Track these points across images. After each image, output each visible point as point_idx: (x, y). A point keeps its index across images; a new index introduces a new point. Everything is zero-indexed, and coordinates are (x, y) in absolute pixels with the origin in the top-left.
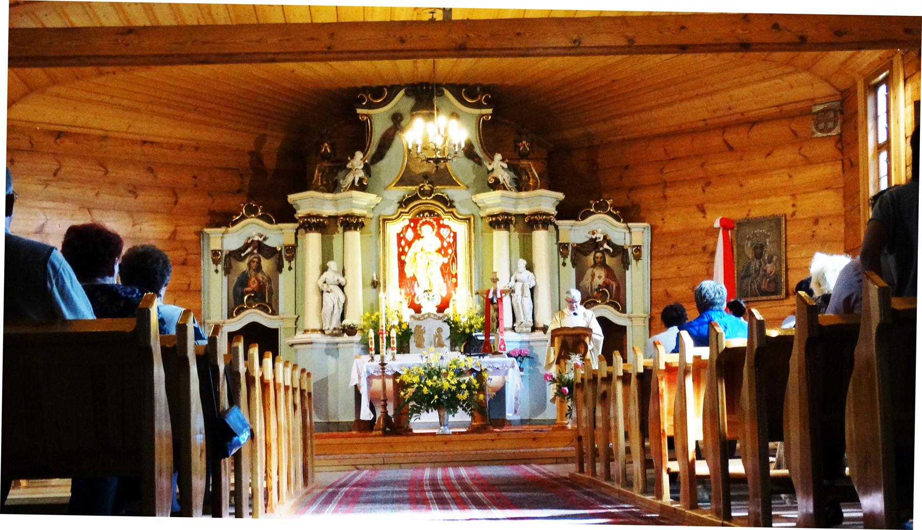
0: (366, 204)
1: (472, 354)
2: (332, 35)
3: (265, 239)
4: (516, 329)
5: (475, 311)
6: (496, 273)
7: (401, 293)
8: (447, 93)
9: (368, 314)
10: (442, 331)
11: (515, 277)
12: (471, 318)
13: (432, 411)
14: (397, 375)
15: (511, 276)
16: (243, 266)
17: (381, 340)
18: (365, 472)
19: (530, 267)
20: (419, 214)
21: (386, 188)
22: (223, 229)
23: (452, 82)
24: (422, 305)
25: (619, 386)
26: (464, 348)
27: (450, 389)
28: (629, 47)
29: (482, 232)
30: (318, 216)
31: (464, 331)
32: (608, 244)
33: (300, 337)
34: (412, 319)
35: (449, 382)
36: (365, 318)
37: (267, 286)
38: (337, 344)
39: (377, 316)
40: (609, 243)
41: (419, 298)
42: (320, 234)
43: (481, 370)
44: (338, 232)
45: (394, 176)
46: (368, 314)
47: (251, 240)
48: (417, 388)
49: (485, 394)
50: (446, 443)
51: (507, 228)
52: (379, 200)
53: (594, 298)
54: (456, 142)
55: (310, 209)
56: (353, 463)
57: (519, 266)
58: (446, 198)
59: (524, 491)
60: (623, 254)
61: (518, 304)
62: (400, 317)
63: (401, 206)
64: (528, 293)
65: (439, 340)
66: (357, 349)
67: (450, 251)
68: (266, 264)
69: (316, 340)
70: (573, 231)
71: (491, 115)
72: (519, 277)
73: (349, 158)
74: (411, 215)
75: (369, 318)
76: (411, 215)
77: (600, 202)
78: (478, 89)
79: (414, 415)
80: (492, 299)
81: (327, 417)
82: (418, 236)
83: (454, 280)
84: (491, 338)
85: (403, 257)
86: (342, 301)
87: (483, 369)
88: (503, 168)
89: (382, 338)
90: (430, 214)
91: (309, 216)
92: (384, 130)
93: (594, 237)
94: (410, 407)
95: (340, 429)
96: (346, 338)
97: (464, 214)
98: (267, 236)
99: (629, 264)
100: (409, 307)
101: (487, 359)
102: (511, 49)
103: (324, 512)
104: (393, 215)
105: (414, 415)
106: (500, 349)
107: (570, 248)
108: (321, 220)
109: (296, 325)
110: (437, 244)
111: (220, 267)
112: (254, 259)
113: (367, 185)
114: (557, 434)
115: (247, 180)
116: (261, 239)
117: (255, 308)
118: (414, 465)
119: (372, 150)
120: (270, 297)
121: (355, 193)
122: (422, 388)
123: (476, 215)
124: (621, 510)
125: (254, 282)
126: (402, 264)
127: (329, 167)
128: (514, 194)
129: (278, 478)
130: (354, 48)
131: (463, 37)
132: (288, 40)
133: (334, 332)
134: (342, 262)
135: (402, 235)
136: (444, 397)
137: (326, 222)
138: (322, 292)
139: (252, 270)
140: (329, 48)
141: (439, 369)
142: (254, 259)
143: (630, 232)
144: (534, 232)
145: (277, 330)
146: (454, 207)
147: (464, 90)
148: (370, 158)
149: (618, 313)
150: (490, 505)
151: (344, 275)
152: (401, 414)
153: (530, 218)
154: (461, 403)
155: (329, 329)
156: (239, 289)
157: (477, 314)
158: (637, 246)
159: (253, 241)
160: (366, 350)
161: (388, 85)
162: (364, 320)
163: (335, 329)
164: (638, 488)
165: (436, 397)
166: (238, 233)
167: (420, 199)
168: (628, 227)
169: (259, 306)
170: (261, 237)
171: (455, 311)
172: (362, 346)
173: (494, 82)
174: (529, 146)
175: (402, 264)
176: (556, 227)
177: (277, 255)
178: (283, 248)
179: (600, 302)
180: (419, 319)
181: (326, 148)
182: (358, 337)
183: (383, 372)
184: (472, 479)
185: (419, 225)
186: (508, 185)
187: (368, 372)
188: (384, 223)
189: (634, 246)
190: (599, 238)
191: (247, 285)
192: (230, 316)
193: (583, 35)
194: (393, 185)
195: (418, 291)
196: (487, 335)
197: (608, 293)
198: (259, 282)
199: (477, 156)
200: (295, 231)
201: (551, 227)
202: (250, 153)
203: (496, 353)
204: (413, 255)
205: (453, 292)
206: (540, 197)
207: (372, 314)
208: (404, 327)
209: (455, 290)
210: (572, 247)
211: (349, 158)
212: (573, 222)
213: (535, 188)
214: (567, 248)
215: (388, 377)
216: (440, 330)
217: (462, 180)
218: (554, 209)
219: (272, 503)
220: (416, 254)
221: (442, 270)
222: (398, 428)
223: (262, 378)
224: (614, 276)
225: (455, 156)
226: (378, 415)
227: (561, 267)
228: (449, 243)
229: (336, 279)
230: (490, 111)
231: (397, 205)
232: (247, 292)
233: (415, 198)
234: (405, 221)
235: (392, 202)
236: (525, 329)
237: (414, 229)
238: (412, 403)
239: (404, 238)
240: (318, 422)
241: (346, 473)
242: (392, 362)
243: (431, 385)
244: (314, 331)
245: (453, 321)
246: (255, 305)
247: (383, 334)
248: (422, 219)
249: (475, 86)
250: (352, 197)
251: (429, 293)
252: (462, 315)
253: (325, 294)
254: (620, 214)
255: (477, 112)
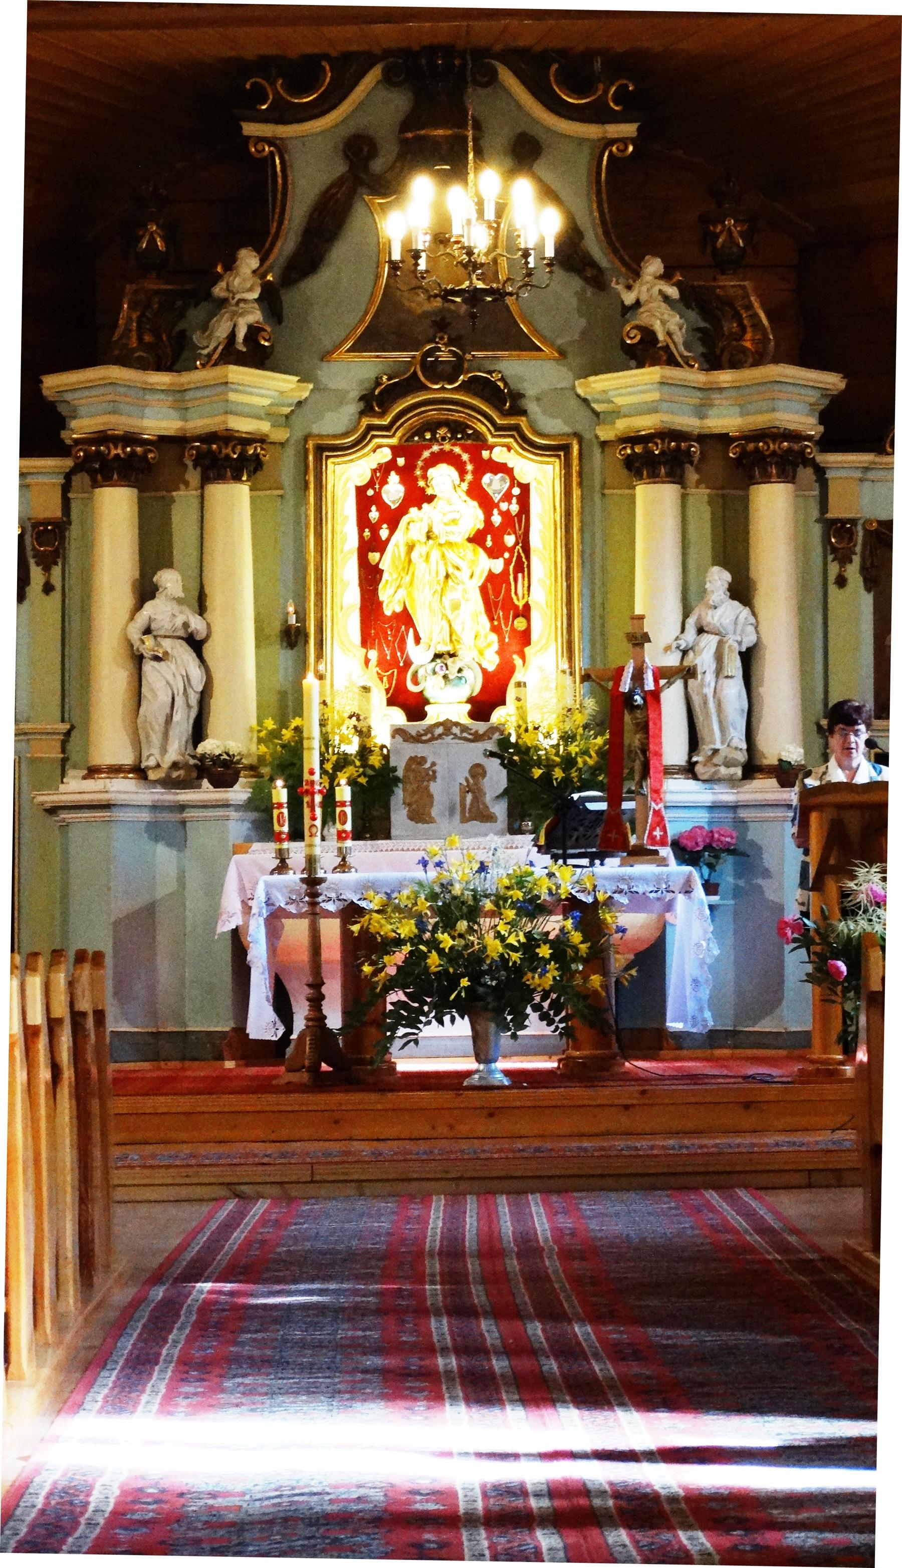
0: (266, 402)
4: (699, 769)
5: (580, 719)
6: (641, 618)
8: (507, 78)
9: (270, 724)
11: (699, 619)
12: (567, 738)
13: (453, 1020)
15: (686, 615)
17: (307, 812)
18: (260, 1207)
21: (325, 356)
24: (427, 694)
29: (604, 486)
30: (130, 439)
34: (399, 739)
36: (263, 734)
38: (182, 807)
39: (298, 730)
41: (420, 674)
42: (135, 491)
44: (187, 484)
45: (351, 319)
46: (270, 724)
49: (605, 973)
50: (491, 1115)
51: (676, 477)
52: (305, 391)
54: (528, 240)
55: (104, 419)
56: (227, 1180)
57: (708, 586)
59: (710, 1327)
61: (705, 697)
62: (363, 733)
63: (367, 411)
64: (734, 666)
65: (476, 799)
67: (510, 540)
70: (867, 485)
71: (633, 141)
72: (713, 618)
73: (219, 269)
74: (399, 434)
75: (275, 734)
76: (399, 434)
78: (598, 65)
79: (401, 1031)
80: (630, 695)
83: (520, 624)
85: (374, 557)
87: (601, 897)
88: (666, 298)
90: (454, 432)
91: (103, 438)
94: (389, 1007)
96: (206, 792)
97: (553, 431)
100: (391, 702)
101: (612, 866)
104: (346, 434)
105: (401, 1031)
106: (652, 838)
109: (63, 751)
113: (272, 346)
118: (400, 1187)
121: (236, 373)
122: (425, 956)
123: (587, 436)
128: (696, 376)
129: (8, 1303)
133: (175, 775)
135: (370, 492)
136: (487, 979)
137: (150, 456)
138: (138, 660)
141: (475, 897)
144: (754, 489)
147: (555, 66)
150: (618, 1396)
152: (364, 1024)
153: (743, 447)
154: (537, 999)
155: (158, 766)
157: (586, 727)
162: (260, 741)
163: (175, 765)
165: (465, 982)
172: (254, 815)
174: (741, 234)
176: (820, 472)
180: (417, 739)
182: (240, 793)
183: (313, 904)
184: (566, 1254)
186: (682, 348)
187: (268, 903)
188: (318, 460)
194: (348, 346)
199: (593, 264)
201: (806, 474)
203: (639, 853)
204: (403, 550)
207: (283, 723)
208: (375, 760)
209: (523, 657)
210: (865, 529)
211: (219, 269)
212: (867, 458)
213: (759, 360)
215: (328, 914)
216: (477, 771)
217: (547, 333)
218: (813, 420)
220: (411, 548)
221: (483, 589)
225: (526, 285)
226: (299, 1024)
227: (832, 589)
228: (505, 515)
229: (179, 621)
230: (629, 129)
233: (410, 385)
235: (340, 398)
236: (723, 770)
238: (396, 996)
239: (377, 499)
241: (205, 1208)
243: (452, 948)
244: (115, 770)
245: (516, 745)
249: (588, 56)
251: (450, 661)
253: (149, 667)
255: (592, 131)
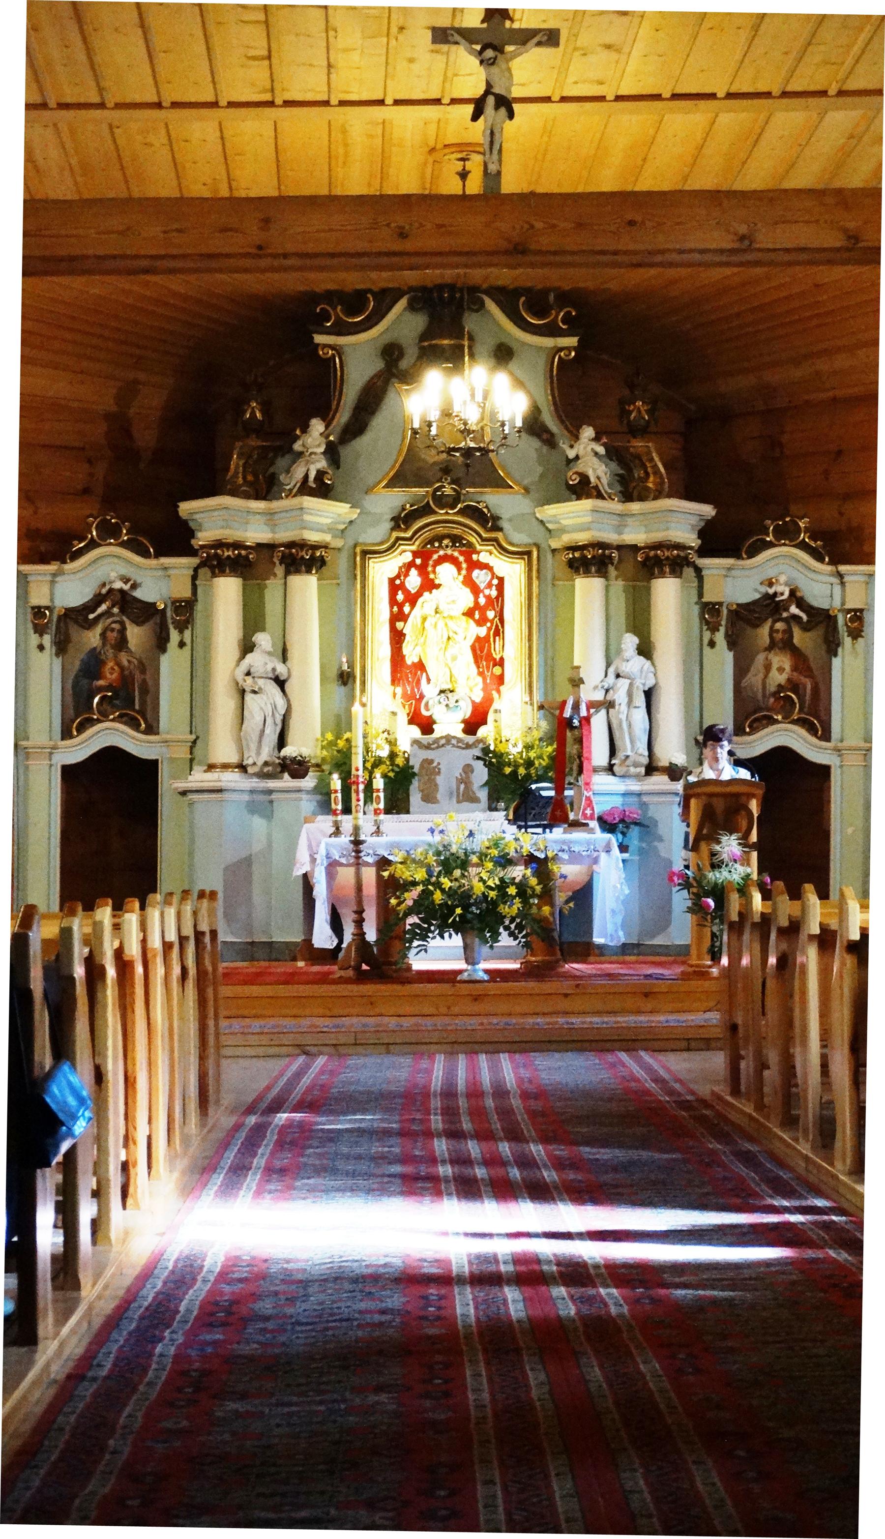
0: (329, 521)
1: (530, 823)
2: (267, 221)
3: (134, 586)
4: (615, 768)
5: (537, 734)
6: (578, 668)
7: (395, 695)
8: (491, 306)
9: (330, 736)
10: (472, 771)
11: (617, 668)
12: (528, 747)
14: (383, 863)
15: (608, 665)
16: (93, 638)
17: (354, 796)
18: (321, 1061)
19: (645, 650)
20: (431, 541)
21: (369, 491)
22: (53, 567)
23: (500, 283)
24: (435, 717)
25: (810, 957)
26: (514, 813)
27: (485, 896)
28: (848, 250)
31: (514, 773)
32: (799, 606)
33: (199, 778)
35: (484, 882)
37: (138, 676)
38: (270, 792)
39: (348, 741)
40: (801, 603)
43: (547, 857)
44: (275, 575)
45: (386, 468)
46: (330, 736)
47: (107, 587)
48: (423, 891)
50: (476, 1000)
51: (602, 572)
52: (354, 514)
53: (768, 710)
58: (485, 510)
59: (620, 1146)
60: (827, 627)
62: (392, 743)
63: (396, 527)
64: (640, 700)
65: (466, 788)
66: (308, 804)
68: (136, 635)
69: (232, 785)
71: (575, 348)
72: (625, 668)
73: (298, 432)
74: (417, 543)
75: (332, 744)
76: (417, 543)
77: (785, 523)
78: (552, 297)
79: (416, 943)
80: (570, 719)
81: (250, 933)
82: (429, 585)
83: (497, 670)
84: (567, 793)
85: (399, 625)
86: (282, 710)
87: (550, 855)
89: (357, 792)
91: (220, 544)
92: (366, 378)
93: (771, 591)
94: (408, 927)
95: (274, 956)
96: (287, 781)
98: (139, 581)
99: (838, 645)
100: (411, 722)
101: (558, 833)
102: (615, 253)
103: (236, 1196)
104: (382, 543)
106: (584, 815)
107: (725, 612)
108: (243, 552)
109: (191, 753)
110: (466, 599)
111: (47, 640)
112: (114, 626)
114: (694, 984)
115: (101, 469)
116: (126, 587)
117: (113, 720)
119: (343, 417)
120: (143, 703)
121: (309, 502)
122: (432, 893)
123: (543, 546)
124: (809, 1218)
125: (112, 669)
126: (397, 638)
127: (258, 447)
128: (616, 506)
130: (310, 248)
131: (522, 227)
132: (179, 231)
133: (266, 770)
134: (281, 633)
135: (398, 582)
136: (474, 909)
138: (242, 692)
139: (108, 647)
140: (260, 248)
141: (465, 853)
142: (114, 626)
143: (843, 584)
145: (155, 763)
146: (500, 529)
147: (523, 299)
148: (338, 430)
149: (814, 740)
151: (284, 659)
152: (391, 938)
154: (507, 922)
155: (255, 764)
156: (85, 682)
157: (541, 740)
158: (855, 610)
159: (111, 590)
160: (325, 807)
161: (375, 289)
162: (323, 748)
163: (266, 764)
164: (844, 1161)
165: (459, 911)
166: (80, 575)
167: (435, 513)
168: (838, 572)
169: (121, 716)
170: (126, 583)
171: (499, 733)
172: (319, 797)
173: (582, 285)
174: (647, 411)
175: (397, 638)
176: (698, 571)
177: (157, 619)
178: (169, 605)
179: (780, 717)
180: (428, 747)
181: (254, 411)
182: (309, 782)
183: (358, 858)
185: (431, 562)
187: (328, 857)
189: (849, 611)
190: (782, 594)
191: (99, 676)
192: (66, 734)
193: (759, 225)
195: (429, 691)
196: (560, 789)
197: (796, 700)
198: (122, 668)
199: (547, 431)
200: (191, 572)
201: (689, 572)
202: (108, 417)
203: (576, 825)
204: (419, 621)
205: (495, 694)
206: (670, 514)
207: (338, 737)
208: (400, 761)
209: (499, 692)
211: (298, 432)
212: (730, 561)
214: (718, 612)
218: (694, 536)
219: (136, 1191)
220: (424, 619)
222: (385, 963)
223: (119, 954)
224: (809, 669)
225: (503, 445)
226: (348, 938)
227: (707, 650)
228: (488, 597)
229: (269, 667)
230: (573, 341)
231: (388, 525)
232: (100, 689)
233: (426, 510)
234: (404, 556)
236: (632, 770)
237: (423, 570)
238: (413, 919)
239: (402, 587)
240: (235, 943)
242: (375, 839)
243: (450, 888)
244: (225, 767)
245: (494, 752)
246: (113, 713)
247: (358, 784)
248: (437, 552)
249: (546, 292)
250: (302, 509)
251: (450, 695)
252: (512, 742)
253: (249, 697)
254: (824, 547)
255: (549, 342)
